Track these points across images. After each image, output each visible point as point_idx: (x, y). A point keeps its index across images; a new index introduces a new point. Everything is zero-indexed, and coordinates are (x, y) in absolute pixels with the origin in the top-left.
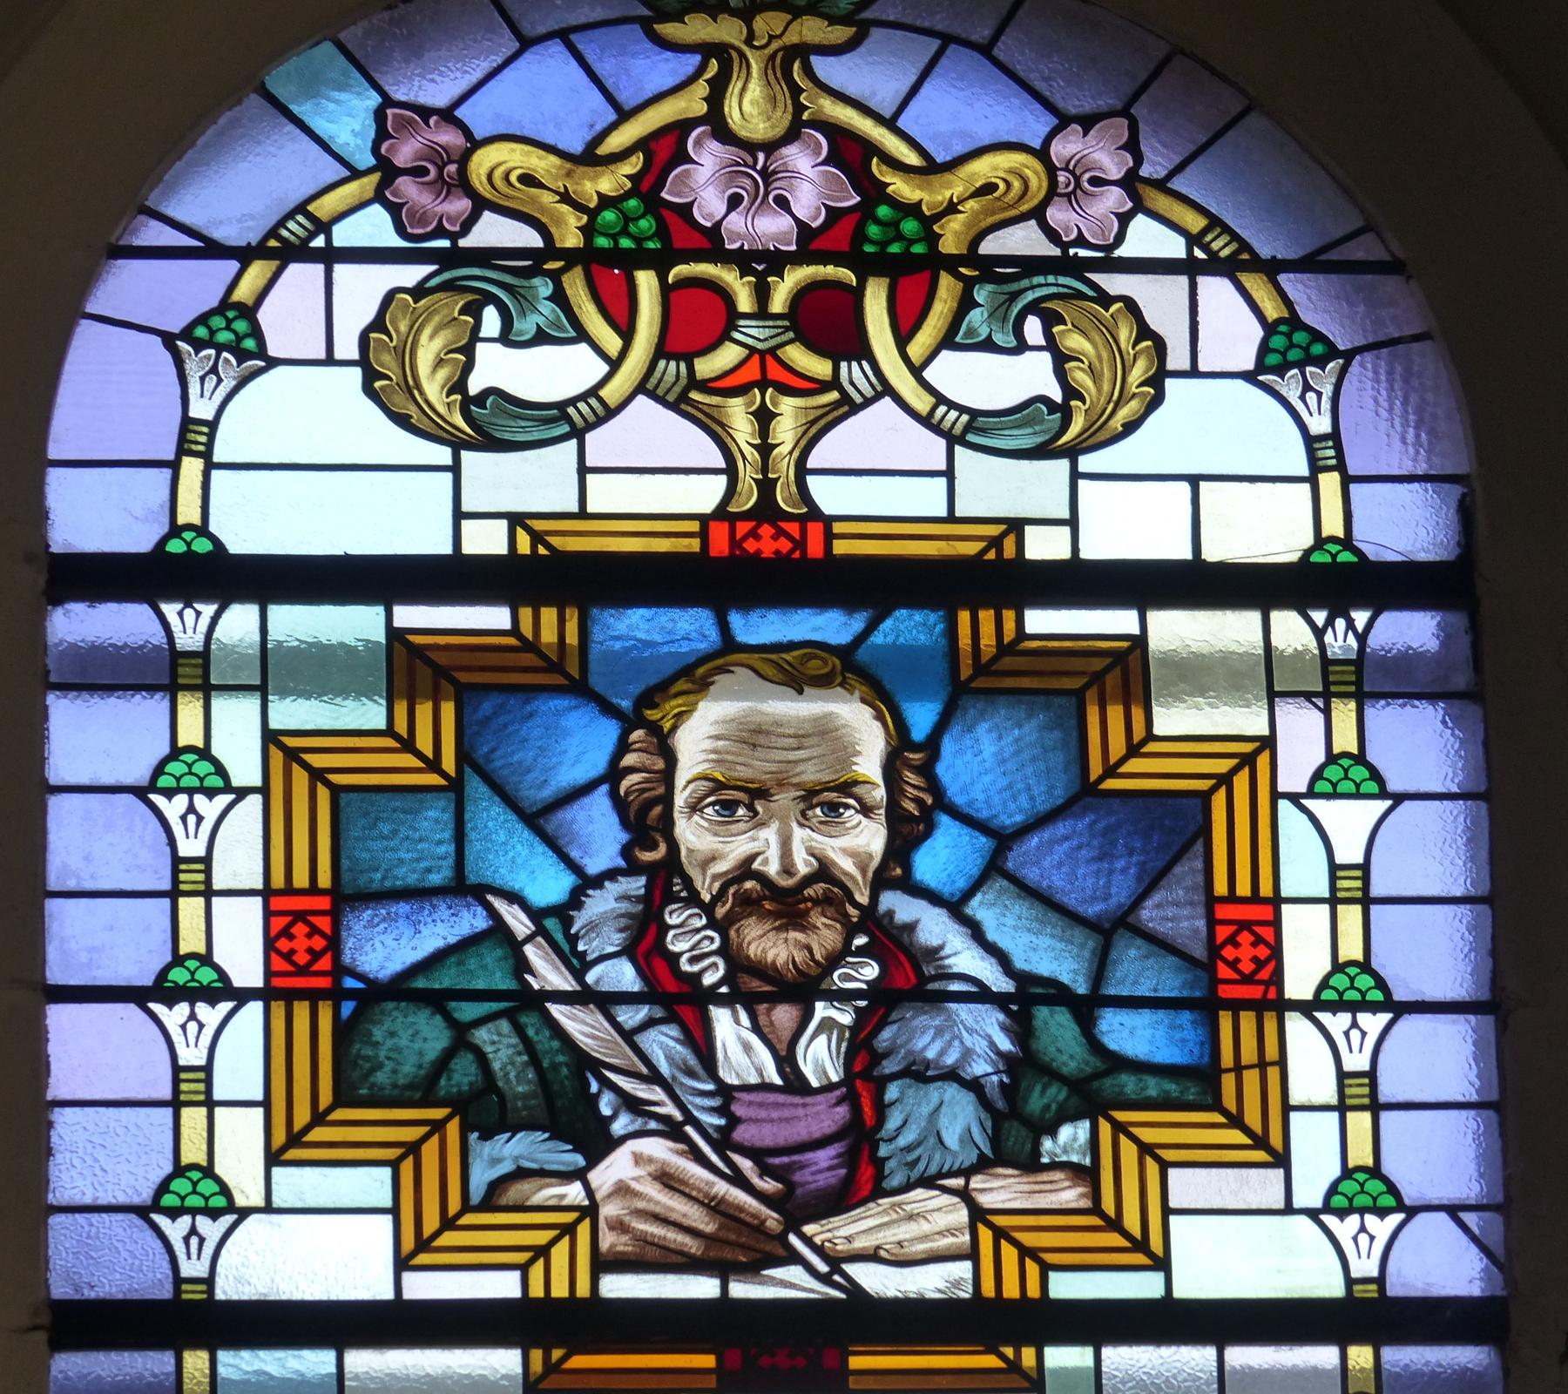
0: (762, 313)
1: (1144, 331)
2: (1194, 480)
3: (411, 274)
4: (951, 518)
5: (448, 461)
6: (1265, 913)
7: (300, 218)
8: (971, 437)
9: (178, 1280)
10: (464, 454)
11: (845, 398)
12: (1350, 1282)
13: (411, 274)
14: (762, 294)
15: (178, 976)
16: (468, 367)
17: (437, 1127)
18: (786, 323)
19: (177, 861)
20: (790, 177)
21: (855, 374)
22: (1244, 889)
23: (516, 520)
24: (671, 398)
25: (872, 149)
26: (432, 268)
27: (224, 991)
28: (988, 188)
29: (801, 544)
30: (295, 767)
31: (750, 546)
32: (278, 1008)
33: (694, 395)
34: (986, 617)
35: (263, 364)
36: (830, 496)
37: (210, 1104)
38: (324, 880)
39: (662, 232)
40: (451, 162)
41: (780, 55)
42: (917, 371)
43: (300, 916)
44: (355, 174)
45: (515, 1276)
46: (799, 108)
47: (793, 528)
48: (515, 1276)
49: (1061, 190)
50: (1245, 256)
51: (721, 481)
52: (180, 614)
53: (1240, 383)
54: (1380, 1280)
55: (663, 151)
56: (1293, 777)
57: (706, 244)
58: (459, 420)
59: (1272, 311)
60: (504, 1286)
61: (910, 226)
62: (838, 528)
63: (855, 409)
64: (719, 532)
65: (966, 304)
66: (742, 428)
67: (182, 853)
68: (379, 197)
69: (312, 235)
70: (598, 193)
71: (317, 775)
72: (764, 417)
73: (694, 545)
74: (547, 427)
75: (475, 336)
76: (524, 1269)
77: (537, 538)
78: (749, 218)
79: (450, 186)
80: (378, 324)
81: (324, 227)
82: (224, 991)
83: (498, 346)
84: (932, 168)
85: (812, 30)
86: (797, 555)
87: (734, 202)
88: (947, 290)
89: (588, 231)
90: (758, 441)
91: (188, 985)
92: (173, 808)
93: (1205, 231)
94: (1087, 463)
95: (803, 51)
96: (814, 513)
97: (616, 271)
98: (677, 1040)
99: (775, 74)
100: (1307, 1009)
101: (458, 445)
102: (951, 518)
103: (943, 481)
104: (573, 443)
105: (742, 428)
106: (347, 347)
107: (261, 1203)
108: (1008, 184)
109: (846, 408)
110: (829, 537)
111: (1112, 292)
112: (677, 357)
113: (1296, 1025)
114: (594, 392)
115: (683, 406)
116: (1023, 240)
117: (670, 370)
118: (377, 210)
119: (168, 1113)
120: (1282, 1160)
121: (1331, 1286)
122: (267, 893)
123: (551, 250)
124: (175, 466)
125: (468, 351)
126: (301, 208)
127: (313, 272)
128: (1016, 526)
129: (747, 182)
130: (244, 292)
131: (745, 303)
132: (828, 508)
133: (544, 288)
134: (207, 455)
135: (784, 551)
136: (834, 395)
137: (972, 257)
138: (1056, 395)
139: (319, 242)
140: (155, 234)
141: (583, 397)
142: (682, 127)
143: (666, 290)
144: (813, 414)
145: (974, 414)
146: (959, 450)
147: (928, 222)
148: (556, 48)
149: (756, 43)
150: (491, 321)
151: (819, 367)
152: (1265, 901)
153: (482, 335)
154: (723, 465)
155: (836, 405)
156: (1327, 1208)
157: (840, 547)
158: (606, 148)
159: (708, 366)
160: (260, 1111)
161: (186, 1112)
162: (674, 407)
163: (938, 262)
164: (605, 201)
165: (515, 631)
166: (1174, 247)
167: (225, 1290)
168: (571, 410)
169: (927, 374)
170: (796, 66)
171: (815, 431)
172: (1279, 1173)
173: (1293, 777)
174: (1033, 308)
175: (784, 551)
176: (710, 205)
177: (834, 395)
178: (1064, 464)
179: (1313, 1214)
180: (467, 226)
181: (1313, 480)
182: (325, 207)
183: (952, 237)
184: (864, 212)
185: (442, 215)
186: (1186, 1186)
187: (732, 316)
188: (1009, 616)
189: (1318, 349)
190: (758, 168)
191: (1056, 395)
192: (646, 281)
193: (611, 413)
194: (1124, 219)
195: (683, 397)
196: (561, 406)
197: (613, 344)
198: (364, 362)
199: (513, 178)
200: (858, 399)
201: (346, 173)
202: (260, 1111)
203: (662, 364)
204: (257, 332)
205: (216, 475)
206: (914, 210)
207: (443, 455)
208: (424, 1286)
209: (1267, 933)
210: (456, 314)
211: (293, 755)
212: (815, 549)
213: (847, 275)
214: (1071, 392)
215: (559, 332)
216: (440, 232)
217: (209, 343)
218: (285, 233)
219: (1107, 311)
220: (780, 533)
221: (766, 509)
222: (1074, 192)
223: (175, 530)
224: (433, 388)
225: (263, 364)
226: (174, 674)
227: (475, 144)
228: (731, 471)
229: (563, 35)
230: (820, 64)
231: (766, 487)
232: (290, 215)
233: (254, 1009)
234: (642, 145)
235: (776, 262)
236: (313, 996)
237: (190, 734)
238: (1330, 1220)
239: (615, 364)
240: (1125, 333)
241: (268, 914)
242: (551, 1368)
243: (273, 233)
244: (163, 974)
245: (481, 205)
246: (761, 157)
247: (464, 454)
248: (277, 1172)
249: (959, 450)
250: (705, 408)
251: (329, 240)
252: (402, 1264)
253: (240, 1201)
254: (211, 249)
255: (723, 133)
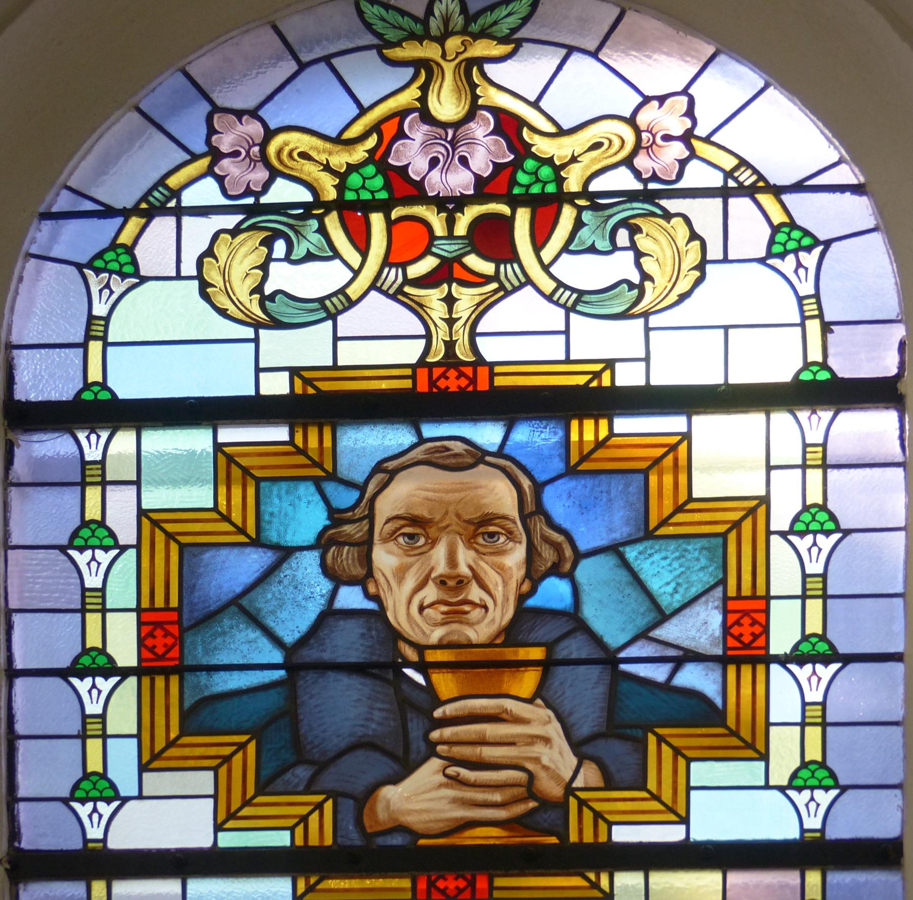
0: (450, 236)
1: (694, 236)
2: (726, 328)
3: (231, 221)
4: (568, 361)
5: (253, 336)
6: (761, 605)
7: (161, 189)
8: (578, 308)
9: (86, 841)
10: (261, 331)
11: (502, 287)
12: (803, 831)
13: (231, 221)
14: (451, 223)
15: (86, 661)
16: (265, 278)
17: (242, 746)
18: (467, 241)
19: (85, 717)
20: (470, 143)
21: (509, 271)
22: (746, 591)
23: (294, 372)
24: (391, 292)
25: (519, 122)
26: (241, 217)
27: (110, 670)
28: (597, 146)
29: (473, 381)
30: (157, 530)
31: (442, 384)
32: (146, 681)
33: (407, 289)
34: (589, 424)
35: (138, 281)
36: (490, 350)
37: (104, 737)
38: (174, 603)
39: (387, 186)
40: (254, 145)
41: (463, 64)
42: (546, 268)
43: (158, 624)
44: (195, 157)
45: (287, 834)
46: (475, 97)
47: (469, 371)
48: (287, 834)
49: (644, 144)
50: (761, 184)
51: (422, 343)
52: (88, 438)
53: (755, 264)
54: (822, 830)
55: (389, 129)
56: (780, 520)
57: (414, 192)
58: (258, 312)
59: (778, 217)
60: (282, 839)
61: (546, 172)
62: (498, 369)
63: (508, 294)
64: (423, 374)
65: (579, 224)
66: (438, 311)
67: (89, 836)
68: (210, 172)
69: (169, 200)
70: (347, 163)
71: (170, 536)
72: (450, 300)
73: (407, 384)
74: (312, 314)
75: (269, 259)
76: (292, 829)
77: (307, 382)
78: (444, 175)
79: (256, 161)
80: (209, 252)
81: (176, 194)
82: (110, 670)
83: (285, 264)
84: (561, 132)
85: (481, 48)
86: (470, 389)
87: (434, 162)
88: (568, 214)
89: (341, 188)
90: (447, 316)
91: (91, 666)
92: (82, 559)
93: (736, 168)
94: (654, 321)
95: (480, 62)
96: (480, 360)
97: (359, 214)
98: (505, 525)
99: (461, 80)
100: (783, 661)
101: (257, 325)
102: (568, 361)
103: (563, 337)
104: (330, 323)
105: (438, 311)
106: (189, 268)
107: (136, 793)
108: (610, 141)
109: (502, 293)
110: (492, 375)
111: (672, 211)
112: (397, 265)
113: (775, 668)
114: (342, 291)
115: (400, 297)
116: (623, 180)
117: (392, 276)
118: (210, 182)
119: (78, 742)
120: (764, 757)
121: (792, 833)
122: (139, 610)
123: (318, 202)
124: (84, 346)
125: (264, 267)
126: (162, 182)
127: (171, 221)
128: (610, 364)
129: (443, 150)
130: (125, 238)
131: (439, 229)
132: (489, 357)
133: (314, 224)
134: (104, 339)
135: (463, 386)
136: (494, 286)
137: (585, 193)
138: (636, 278)
139: (172, 204)
140: (64, 202)
141: (335, 294)
142: (402, 114)
143: (390, 224)
144: (478, 299)
145: (581, 293)
146: (573, 316)
147: (558, 169)
148: (322, 66)
149: (448, 58)
150: (280, 247)
151: (487, 268)
152: (761, 598)
153: (274, 256)
154: (424, 333)
155: (496, 291)
156: (790, 786)
157: (499, 381)
158: (348, 135)
159: (417, 270)
160: (135, 741)
161: (89, 742)
162: (393, 297)
163: (562, 198)
164: (352, 168)
165: (291, 442)
166: (716, 180)
167: (112, 844)
168: (328, 303)
169: (552, 270)
170: (475, 69)
171: (482, 309)
172: (762, 764)
173: (780, 520)
174: (623, 223)
175: (463, 386)
176: (418, 166)
177: (494, 286)
178: (641, 321)
179: (782, 789)
180: (266, 186)
181: (802, 325)
182: (173, 182)
183: (573, 184)
184: (517, 165)
185: (250, 181)
186: (701, 772)
187: (432, 237)
188: (299, 842)
189: (807, 241)
190: (449, 139)
191: (636, 278)
192: (377, 220)
193: (352, 304)
194: (683, 163)
195: (400, 290)
196: (321, 300)
197: (354, 259)
198: (200, 277)
199: (295, 155)
200: (509, 287)
201: (188, 157)
202: (135, 741)
203: (386, 270)
204: (134, 262)
205: (110, 349)
206: (549, 161)
207: (249, 333)
208: (227, 840)
209: (761, 617)
210: (257, 245)
211: (155, 523)
212: (483, 386)
213: (505, 209)
214: (646, 276)
215: (322, 253)
216: (248, 192)
217: (105, 270)
218: (151, 199)
219: (669, 222)
220: (461, 375)
221: (450, 359)
222: (651, 146)
223: (87, 386)
224: (242, 290)
225: (138, 281)
226: (83, 475)
227: (270, 134)
228: (428, 337)
229: (327, 60)
230: (489, 68)
231: (450, 345)
232: (154, 187)
233: (132, 681)
234: (376, 128)
235: (458, 203)
236: (167, 673)
237: (93, 512)
238: (792, 793)
239: (356, 273)
240: (682, 233)
241: (140, 624)
242: (310, 889)
243: (144, 198)
244: (76, 660)
245: (275, 174)
246: (450, 132)
247: (261, 331)
248: (146, 776)
249: (573, 316)
250: (415, 298)
251: (179, 201)
252: (687, 437)
253: (123, 793)
254: (108, 212)
255: (427, 117)
